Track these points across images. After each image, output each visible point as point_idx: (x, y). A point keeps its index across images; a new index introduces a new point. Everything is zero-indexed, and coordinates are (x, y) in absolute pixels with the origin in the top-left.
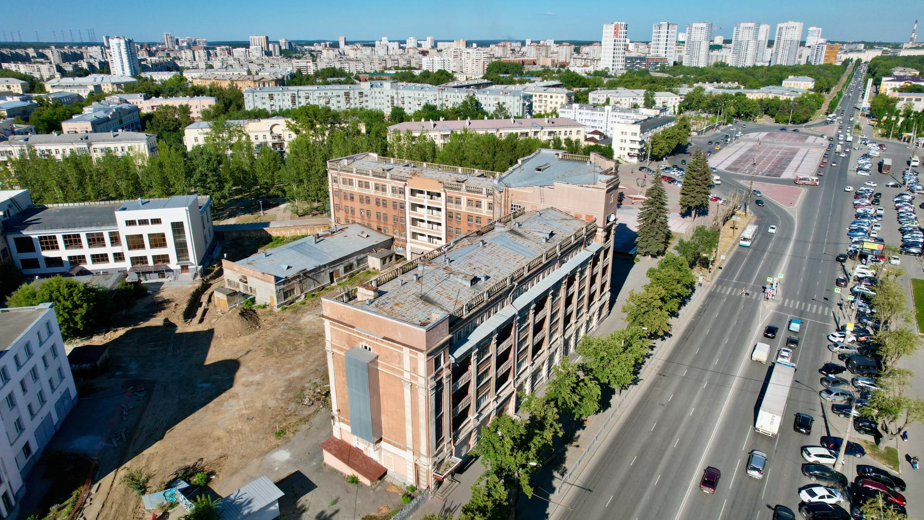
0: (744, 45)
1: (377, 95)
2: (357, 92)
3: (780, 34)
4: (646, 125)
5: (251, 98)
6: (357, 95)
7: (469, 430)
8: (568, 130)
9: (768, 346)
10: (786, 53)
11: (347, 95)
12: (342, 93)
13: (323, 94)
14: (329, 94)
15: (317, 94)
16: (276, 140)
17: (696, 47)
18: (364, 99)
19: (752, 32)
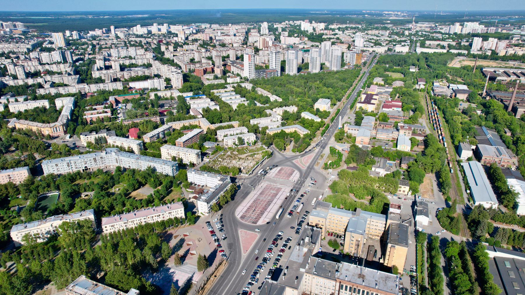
0: (315, 59)
1: (109, 157)
2: (99, 157)
3: (332, 52)
4: (208, 201)
5: (46, 167)
6: (99, 158)
7: (154, 134)
8: (177, 210)
9: (427, 225)
10: (336, 61)
11: (95, 159)
12: (92, 159)
13: (83, 161)
14: (86, 160)
15: (80, 161)
16: (54, 229)
17: (291, 62)
18: (103, 159)
19: (318, 53)
